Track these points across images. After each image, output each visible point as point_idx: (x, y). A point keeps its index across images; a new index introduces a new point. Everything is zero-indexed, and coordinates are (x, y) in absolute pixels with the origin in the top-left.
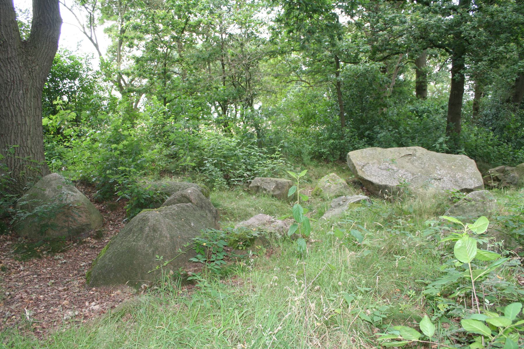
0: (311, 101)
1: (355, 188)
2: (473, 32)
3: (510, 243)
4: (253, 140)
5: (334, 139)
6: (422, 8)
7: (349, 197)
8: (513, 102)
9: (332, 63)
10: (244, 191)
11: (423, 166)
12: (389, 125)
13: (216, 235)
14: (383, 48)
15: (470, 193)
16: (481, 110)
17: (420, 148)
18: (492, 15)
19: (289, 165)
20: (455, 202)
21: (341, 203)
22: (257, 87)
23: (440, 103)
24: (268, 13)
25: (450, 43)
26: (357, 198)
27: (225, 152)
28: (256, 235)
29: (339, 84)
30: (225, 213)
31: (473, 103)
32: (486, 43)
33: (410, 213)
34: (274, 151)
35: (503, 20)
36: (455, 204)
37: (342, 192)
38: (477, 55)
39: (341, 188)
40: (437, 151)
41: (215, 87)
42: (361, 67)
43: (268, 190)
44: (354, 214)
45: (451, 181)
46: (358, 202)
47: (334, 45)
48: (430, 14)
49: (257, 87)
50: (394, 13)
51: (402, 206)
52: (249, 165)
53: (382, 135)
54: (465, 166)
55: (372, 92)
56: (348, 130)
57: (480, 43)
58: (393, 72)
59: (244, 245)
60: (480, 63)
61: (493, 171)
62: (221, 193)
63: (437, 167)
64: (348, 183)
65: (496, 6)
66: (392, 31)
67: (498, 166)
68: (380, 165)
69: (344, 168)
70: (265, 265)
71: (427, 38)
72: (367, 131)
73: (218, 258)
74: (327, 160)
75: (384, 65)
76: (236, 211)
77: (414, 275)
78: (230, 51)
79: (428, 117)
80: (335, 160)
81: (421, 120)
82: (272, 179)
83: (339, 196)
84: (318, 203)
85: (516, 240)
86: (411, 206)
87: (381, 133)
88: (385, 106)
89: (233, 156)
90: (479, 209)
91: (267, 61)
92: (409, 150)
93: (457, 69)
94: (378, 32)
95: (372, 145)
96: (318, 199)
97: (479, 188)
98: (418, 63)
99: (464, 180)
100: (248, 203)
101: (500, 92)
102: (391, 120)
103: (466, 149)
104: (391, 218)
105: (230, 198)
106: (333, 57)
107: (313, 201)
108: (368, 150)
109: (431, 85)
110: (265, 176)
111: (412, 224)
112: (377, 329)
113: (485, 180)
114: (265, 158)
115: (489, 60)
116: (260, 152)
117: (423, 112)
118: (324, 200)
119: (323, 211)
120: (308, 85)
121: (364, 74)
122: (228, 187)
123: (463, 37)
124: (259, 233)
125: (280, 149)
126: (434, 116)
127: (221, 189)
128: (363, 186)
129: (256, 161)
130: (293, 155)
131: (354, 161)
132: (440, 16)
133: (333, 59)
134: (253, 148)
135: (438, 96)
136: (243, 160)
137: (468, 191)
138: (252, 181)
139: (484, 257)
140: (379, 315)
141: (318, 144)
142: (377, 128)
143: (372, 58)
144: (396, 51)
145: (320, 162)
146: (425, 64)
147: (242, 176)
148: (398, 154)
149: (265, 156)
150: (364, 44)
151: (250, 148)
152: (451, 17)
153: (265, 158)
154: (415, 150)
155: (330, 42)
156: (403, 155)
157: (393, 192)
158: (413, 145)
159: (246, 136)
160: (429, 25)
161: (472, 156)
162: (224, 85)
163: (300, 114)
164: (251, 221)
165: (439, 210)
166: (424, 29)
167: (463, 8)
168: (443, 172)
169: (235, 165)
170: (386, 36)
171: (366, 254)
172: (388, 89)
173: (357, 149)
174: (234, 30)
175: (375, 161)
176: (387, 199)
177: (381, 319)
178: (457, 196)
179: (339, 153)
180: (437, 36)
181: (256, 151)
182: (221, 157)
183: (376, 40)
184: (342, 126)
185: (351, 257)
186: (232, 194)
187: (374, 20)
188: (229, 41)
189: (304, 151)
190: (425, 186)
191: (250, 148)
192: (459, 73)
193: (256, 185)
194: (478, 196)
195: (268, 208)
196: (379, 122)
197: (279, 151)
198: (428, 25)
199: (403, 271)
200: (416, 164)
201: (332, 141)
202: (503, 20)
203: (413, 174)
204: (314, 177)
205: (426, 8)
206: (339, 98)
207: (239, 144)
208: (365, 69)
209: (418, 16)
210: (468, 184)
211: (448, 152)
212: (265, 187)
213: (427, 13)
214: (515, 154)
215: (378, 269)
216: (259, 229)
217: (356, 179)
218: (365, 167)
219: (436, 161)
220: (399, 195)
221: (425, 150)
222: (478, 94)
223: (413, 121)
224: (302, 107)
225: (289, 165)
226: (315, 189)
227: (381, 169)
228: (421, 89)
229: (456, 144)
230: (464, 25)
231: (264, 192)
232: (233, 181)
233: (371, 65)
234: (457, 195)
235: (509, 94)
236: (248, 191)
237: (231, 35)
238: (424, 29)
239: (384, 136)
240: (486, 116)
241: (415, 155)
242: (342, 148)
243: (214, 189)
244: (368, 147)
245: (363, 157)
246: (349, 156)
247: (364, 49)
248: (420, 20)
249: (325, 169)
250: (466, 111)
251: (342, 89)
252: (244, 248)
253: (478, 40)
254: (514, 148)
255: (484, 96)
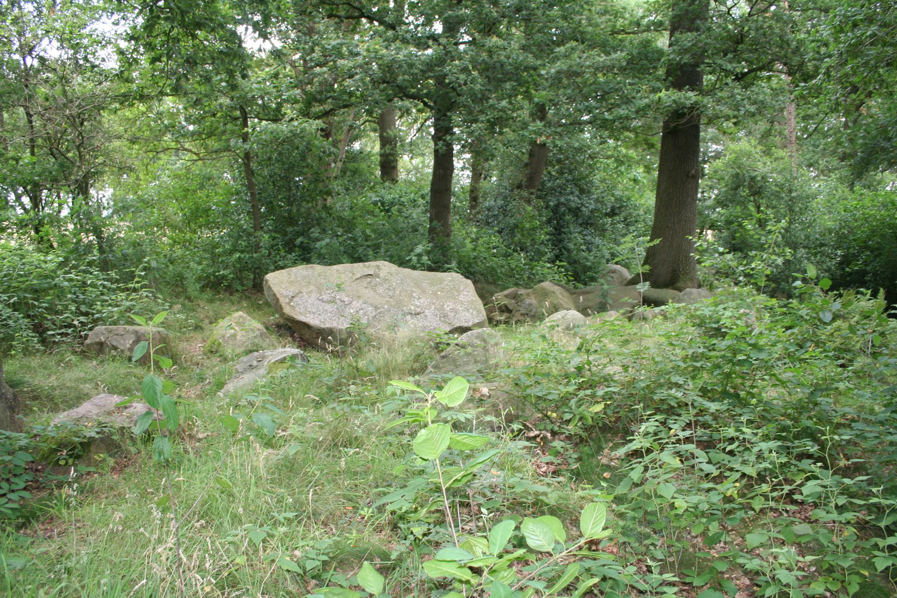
0: (202, 187)
1: (280, 336)
2: (462, 77)
3: (523, 411)
4: (90, 258)
5: (242, 252)
6: (385, 32)
7: (268, 353)
8: (527, 187)
9: (236, 119)
10: (74, 353)
11: (391, 293)
12: (338, 226)
13: (8, 442)
14: (323, 96)
15: (464, 335)
16: (481, 200)
17: (387, 263)
18: (490, 52)
19: (159, 301)
20: (442, 351)
21: (255, 363)
22: (100, 160)
23: (419, 190)
24: (116, 23)
25: (430, 92)
26: (282, 353)
27: (35, 282)
28: (93, 434)
29: (247, 156)
30: (36, 398)
31: (469, 189)
32: (483, 95)
33: (371, 374)
34: (132, 276)
35: (506, 60)
36: (442, 354)
37: (257, 345)
38: (470, 113)
39: (255, 337)
40: (414, 268)
41: (13, 158)
42: (283, 128)
43: (122, 348)
44: (277, 382)
45: (436, 316)
46: (283, 361)
47: (234, 87)
48: (398, 43)
49: (100, 160)
50: (338, 37)
51: (356, 362)
52: (84, 303)
53: (324, 243)
54: (457, 291)
55: (305, 170)
56: (266, 236)
57: (475, 94)
58: (342, 137)
59: (71, 456)
60: (474, 125)
61: (500, 297)
62: (26, 361)
63: (414, 295)
64: (267, 328)
65: (495, 39)
66: (336, 68)
67: (508, 288)
68: (321, 295)
69: (261, 302)
70: (112, 489)
71: (393, 82)
72: (298, 237)
73: (14, 487)
74: (230, 290)
75: (324, 126)
76: (57, 392)
77: (375, 479)
78: (43, 90)
79: (399, 211)
80: (245, 288)
81: (389, 217)
82: (128, 327)
83: (251, 351)
84: (215, 367)
85: (531, 403)
86: (371, 361)
87: (322, 239)
88: (329, 193)
89: (51, 288)
90: (478, 359)
91: (115, 112)
92: (368, 267)
93: (443, 132)
94: (312, 68)
95: (307, 260)
96: (215, 360)
97: (480, 325)
98: (383, 124)
99: (456, 313)
100: (82, 375)
101: (508, 172)
102: (340, 218)
103: (459, 263)
104: (340, 385)
105: (45, 368)
106: (236, 109)
107: (207, 362)
108: (301, 270)
109: (405, 162)
110: (115, 323)
111: (374, 392)
112: (314, 582)
113: (489, 311)
114: (114, 290)
115: (488, 121)
116: (104, 279)
117: (392, 204)
118: (225, 360)
119: (223, 380)
120: (195, 157)
121: (289, 140)
122: (42, 348)
123: (449, 84)
124: (98, 430)
125: (143, 273)
126: (410, 211)
127: (27, 352)
128: (294, 333)
129: (97, 296)
130: (168, 283)
131: (276, 289)
132: (413, 49)
133: (238, 113)
134: (91, 273)
135: (417, 178)
136: (70, 296)
137: (463, 330)
138: (90, 333)
139: (464, 444)
140: (315, 557)
141: (214, 262)
142: (315, 232)
143: (306, 113)
144: (345, 102)
145: (219, 293)
146: (394, 124)
147: (70, 326)
148: (350, 275)
149: (114, 286)
150: (288, 88)
151: (85, 272)
152: (429, 51)
153: (114, 290)
154: (378, 267)
155: (227, 82)
156: (359, 276)
157: (341, 340)
158: (376, 259)
159: (79, 251)
160: (396, 62)
161: (468, 273)
162: (33, 154)
163: (182, 210)
164: (85, 408)
165: (417, 365)
166: (388, 67)
167: (447, 37)
168: (424, 301)
169: (57, 305)
170: (326, 76)
171: (292, 452)
172: (333, 165)
173: (282, 268)
174: (51, 50)
175: (312, 287)
176: (332, 351)
177: (319, 563)
178: (444, 341)
179: (252, 276)
180: (408, 81)
181: (97, 277)
182: (25, 291)
183: (311, 83)
184: (255, 228)
185: (267, 459)
186: (50, 361)
187: (307, 47)
188: (38, 71)
189: (188, 274)
190: (393, 327)
191: (85, 272)
192: (445, 140)
193: (97, 340)
194: (477, 337)
195: (122, 382)
196: (319, 222)
197: (140, 276)
198: (394, 61)
199: (356, 473)
200: (381, 290)
201: (237, 255)
202: (506, 60)
203: (376, 308)
204: (207, 321)
205: (390, 33)
206: (249, 181)
207: (61, 265)
208: (291, 131)
209: (377, 45)
210: (462, 319)
211: (430, 269)
212: (115, 344)
213: (394, 41)
214: (532, 269)
215: (315, 475)
216: (100, 424)
217: (282, 321)
218: (295, 299)
219: (412, 284)
220: (352, 344)
221: (394, 268)
222: (477, 176)
223: (375, 219)
224: (185, 197)
225: (159, 301)
226: (209, 342)
227: (322, 300)
228: (388, 166)
229: (444, 256)
230: (449, 65)
231: (114, 353)
232: (53, 335)
233: (301, 123)
234: (445, 339)
235: (520, 177)
236: (83, 352)
237: (42, 60)
238: (388, 67)
239: (327, 244)
240: (489, 210)
241: (378, 276)
242: (257, 268)
243: (13, 352)
244: (302, 264)
245: (291, 282)
246: (267, 281)
247: (290, 96)
248: (381, 53)
249: (227, 305)
250: (458, 201)
251: (254, 165)
252: (70, 461)
253: (472, 89)
254: (531, 260)
255: (485, 178)
